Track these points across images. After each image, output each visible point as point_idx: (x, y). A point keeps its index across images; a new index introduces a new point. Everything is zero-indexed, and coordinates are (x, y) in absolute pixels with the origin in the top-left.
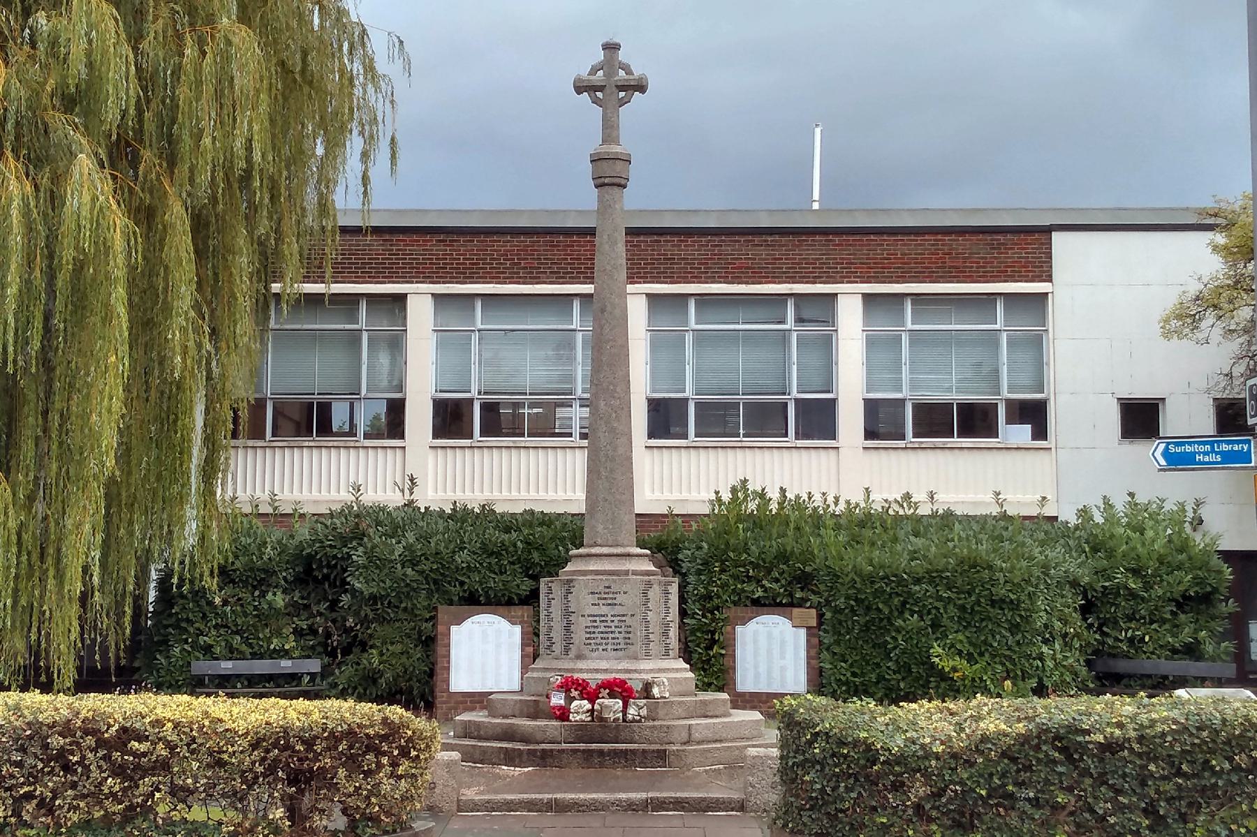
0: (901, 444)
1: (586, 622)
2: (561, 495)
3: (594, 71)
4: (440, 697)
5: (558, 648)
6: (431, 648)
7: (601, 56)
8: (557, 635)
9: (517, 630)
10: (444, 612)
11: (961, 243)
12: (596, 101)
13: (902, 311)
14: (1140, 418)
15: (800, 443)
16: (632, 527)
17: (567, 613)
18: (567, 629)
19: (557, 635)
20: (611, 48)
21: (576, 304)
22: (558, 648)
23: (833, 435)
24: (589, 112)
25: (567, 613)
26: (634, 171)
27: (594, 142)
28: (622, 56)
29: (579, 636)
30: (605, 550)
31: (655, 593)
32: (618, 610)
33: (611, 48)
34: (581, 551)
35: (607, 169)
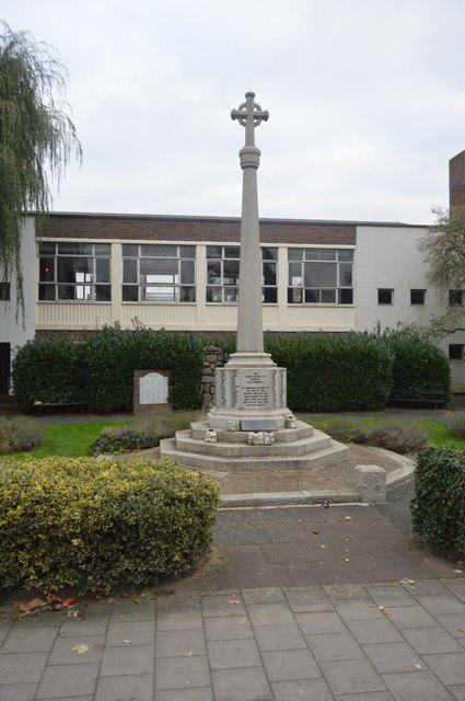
0: (333, 305)
1: (245, 391)
2: (53, 323)
3: (241, 107)
4: (136, 406)
5: (228, 403)
6: (130, 390)
7: (244, 100)
8: (228, 396)
9: (166, 379)
10: (136, 373)
11: (324, 230)
12: (242, 123)
13: (301, 255)
14: (385, 297)
15: (307, 304)
16: (261, 338)
17: (234, 386)
18: (234, 393)
19: (228, 396)
20: (250, 96)
21: (178, 249)
22: (228, 403)
23: (276, 302)
24: (238, 130)
25: (234, 386)
26: (262, 160)
27: (241, 144)
28: (256, 100)
29: (241, 397)
30: (250, 354)
31: (277, 376)
32: (261, 385)
33: (250, 96)
34: (235, 354)
35: (248, 158)
